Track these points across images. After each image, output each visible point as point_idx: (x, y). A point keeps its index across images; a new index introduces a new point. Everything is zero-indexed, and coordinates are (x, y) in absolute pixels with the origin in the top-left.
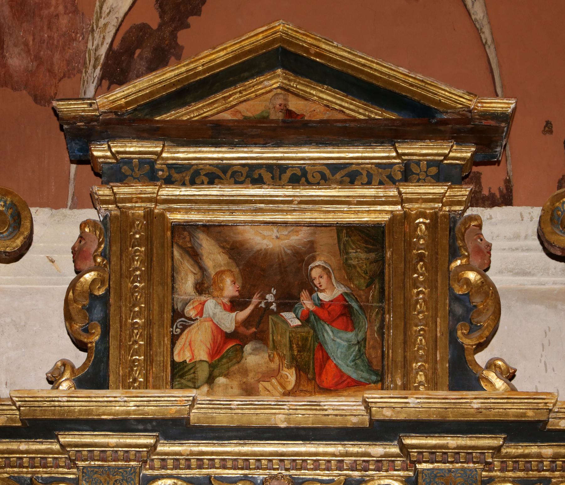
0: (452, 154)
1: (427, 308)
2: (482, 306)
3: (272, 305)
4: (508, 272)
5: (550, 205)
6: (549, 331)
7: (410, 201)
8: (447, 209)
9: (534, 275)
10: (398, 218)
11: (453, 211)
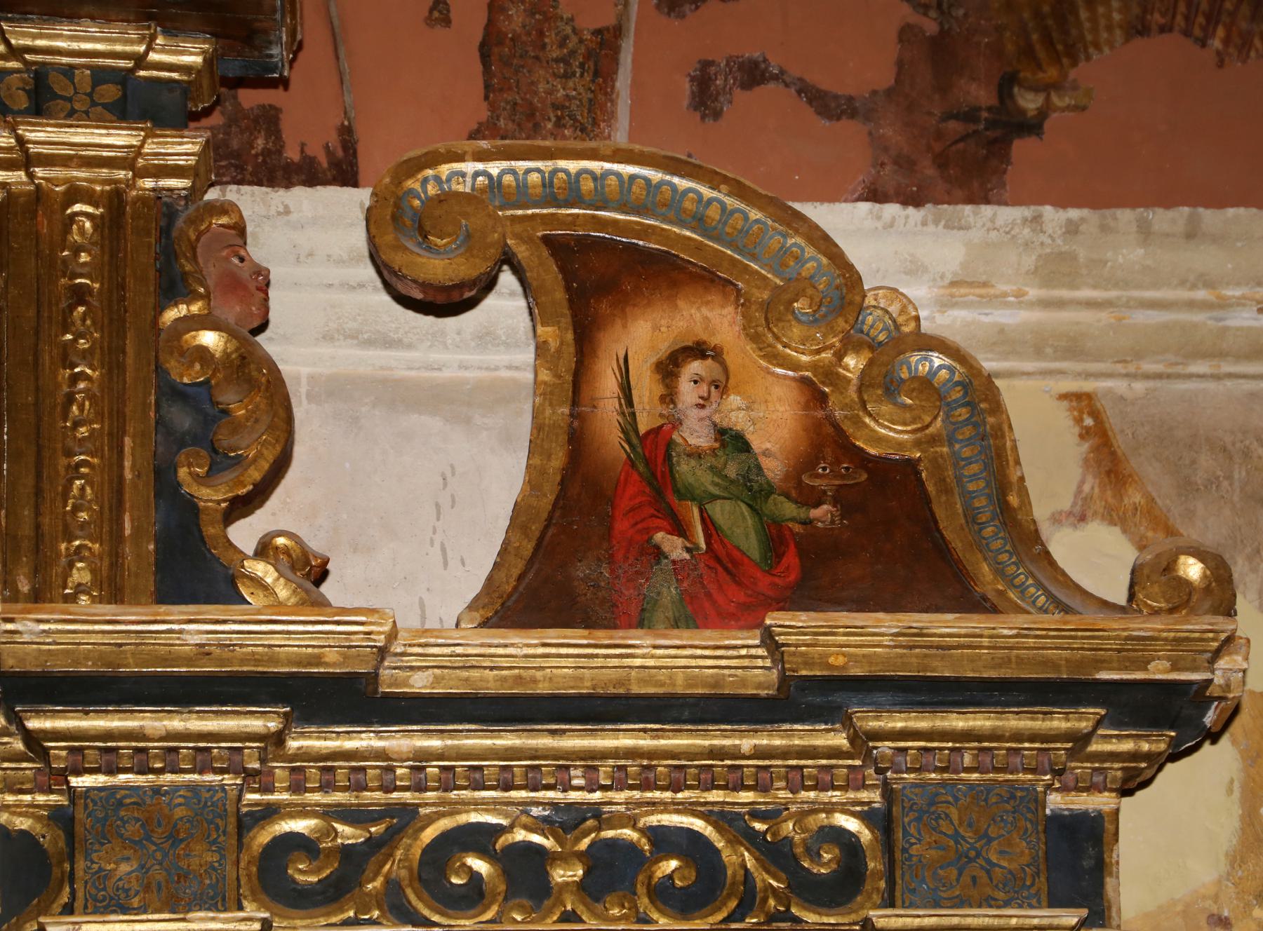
0: (153, 57)
1: (97, 413)
2: (243, 412)
3: (1114, 497)
4: (346, 337)
5: (391, 182)
6: (453, 474)
7: (48, 161)
8: (148, 183)
9: (410, 346)
10: (22, 200)
11: (164, 189)
